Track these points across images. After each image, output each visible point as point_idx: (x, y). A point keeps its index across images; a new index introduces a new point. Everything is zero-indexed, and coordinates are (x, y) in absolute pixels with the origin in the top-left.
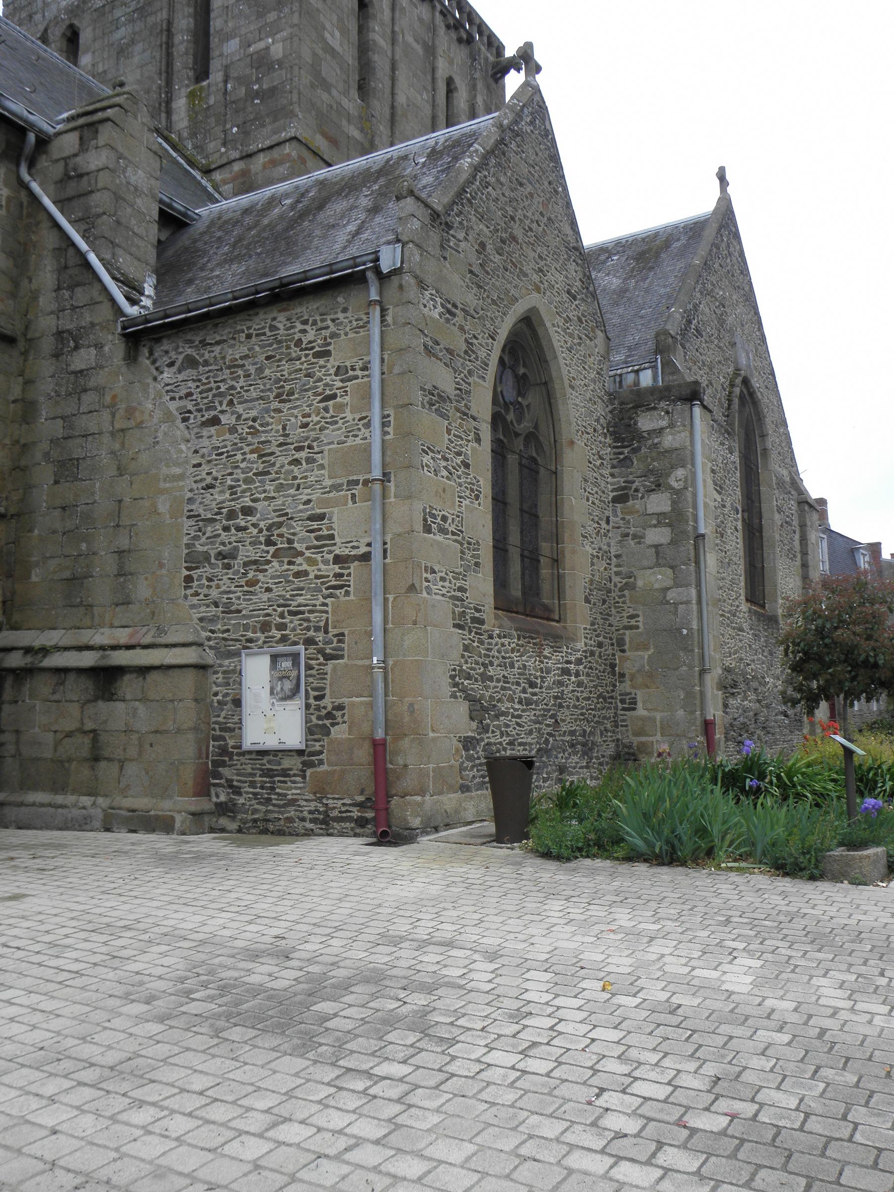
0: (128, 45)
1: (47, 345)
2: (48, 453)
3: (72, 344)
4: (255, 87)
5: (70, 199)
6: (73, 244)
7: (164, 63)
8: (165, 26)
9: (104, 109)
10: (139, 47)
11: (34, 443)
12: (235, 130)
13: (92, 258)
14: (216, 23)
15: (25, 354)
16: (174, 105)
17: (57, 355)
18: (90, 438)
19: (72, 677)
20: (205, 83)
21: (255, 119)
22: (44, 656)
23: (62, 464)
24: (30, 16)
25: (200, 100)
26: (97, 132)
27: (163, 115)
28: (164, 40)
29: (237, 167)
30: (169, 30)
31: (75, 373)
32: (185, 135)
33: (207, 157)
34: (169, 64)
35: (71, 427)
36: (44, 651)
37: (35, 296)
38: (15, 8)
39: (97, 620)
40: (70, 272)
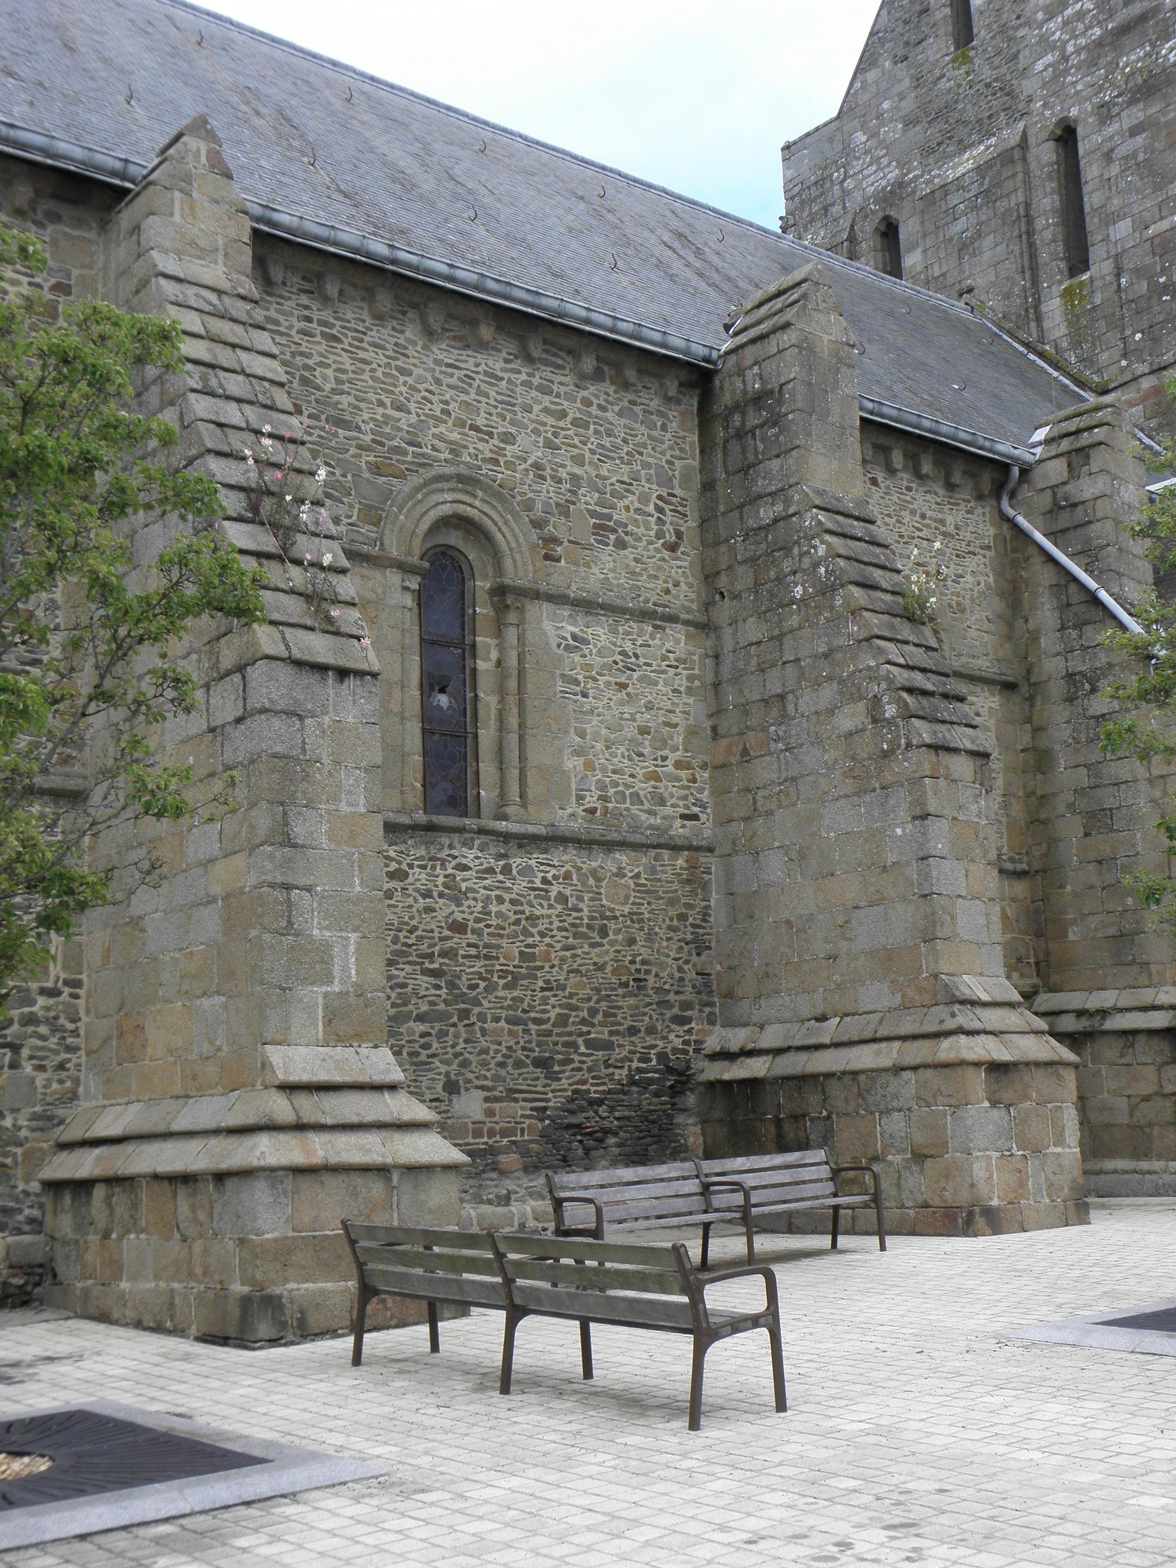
0: (973, 240)
1: (1057, 688)
2: (1073, 804)
3: (1087, 686)
4: (1162, 280)
5: (1064, 531)
6: (1075, 579)
7: (1026, 258)
8: (1022, 212)
9: (1090, 429)
10: (989, 240)
11: (1054, 794)
12: (1138, 336)
13: (1103, 595)
14: (1092, 198)
15: (1031, 699)
16: (1044, 308)
17: (1070, 700)
18: (1123, 787)
19: (1141, 1040)
20: (1085, 277)
21: (1166, 321)
22: (1104, 1019)
23: (1092, 815)
24: (826, 210)
25: (1082, 298)
26: (1088, 457)
27: (1033, 324)
28: (1023, 229)
29: (1146, 384)
30: (1027, 215)
31: (1096, 718)
32: (1065, 345)
33: (1099, 371)
34: (1033, 257)
35: (1098, 775)
36: (1104, 1013)
37: (1034, 636)
38: (802, 202)
39: (1155, 978)
40: (1074, 609)
